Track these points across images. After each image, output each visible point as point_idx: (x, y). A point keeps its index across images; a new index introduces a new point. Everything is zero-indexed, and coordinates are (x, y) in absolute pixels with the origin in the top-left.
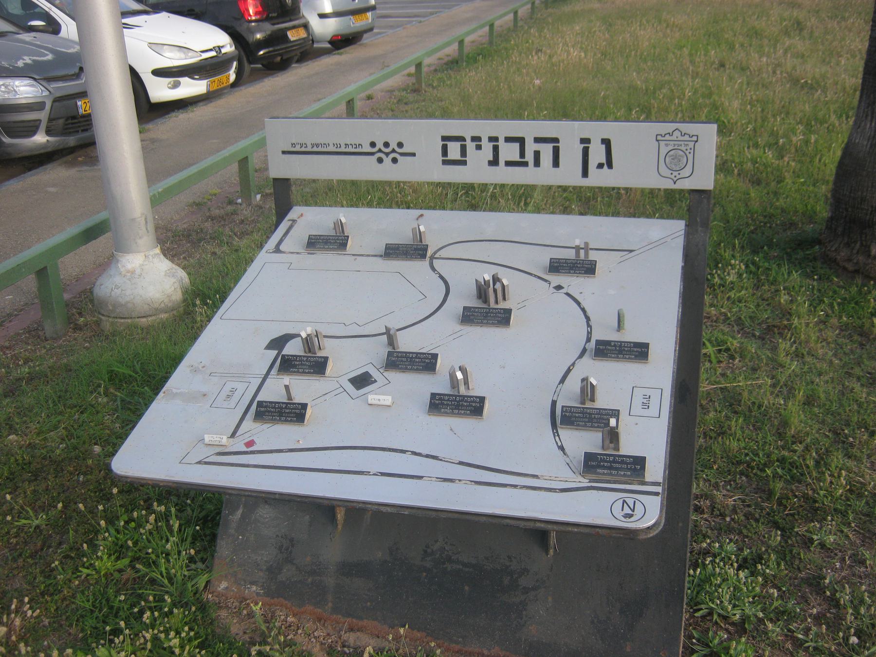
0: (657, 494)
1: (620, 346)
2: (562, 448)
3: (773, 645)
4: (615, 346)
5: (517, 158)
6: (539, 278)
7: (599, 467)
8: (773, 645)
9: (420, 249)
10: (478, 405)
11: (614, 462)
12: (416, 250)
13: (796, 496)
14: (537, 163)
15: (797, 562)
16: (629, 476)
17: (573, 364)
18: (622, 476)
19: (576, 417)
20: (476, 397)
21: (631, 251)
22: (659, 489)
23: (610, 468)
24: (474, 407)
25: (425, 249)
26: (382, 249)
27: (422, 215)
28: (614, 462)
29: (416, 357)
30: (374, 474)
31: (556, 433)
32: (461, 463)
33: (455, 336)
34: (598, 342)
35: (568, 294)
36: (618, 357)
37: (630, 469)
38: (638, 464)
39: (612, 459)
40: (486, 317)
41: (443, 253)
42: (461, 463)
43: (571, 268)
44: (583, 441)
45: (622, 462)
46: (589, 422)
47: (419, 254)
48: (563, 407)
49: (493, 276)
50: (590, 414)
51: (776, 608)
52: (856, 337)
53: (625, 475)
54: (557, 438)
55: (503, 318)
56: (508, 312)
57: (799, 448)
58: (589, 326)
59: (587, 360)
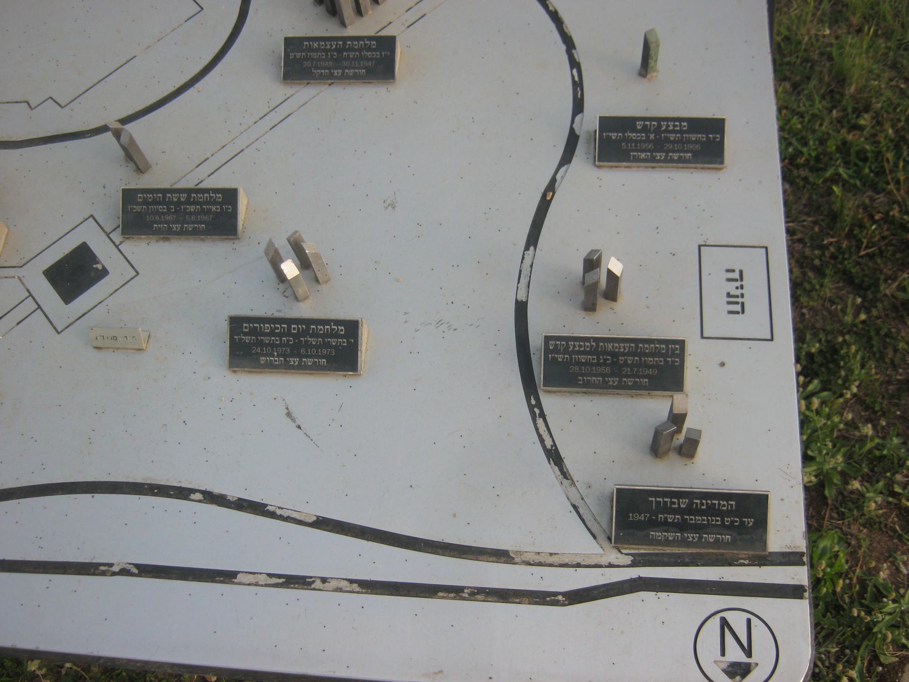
0: (795, 592)
2: (554, 456)
3: (870, 524)
4: (645, 129)
5: (117, 243)
7: (655, 524)
8: (870, 524)
10: (344, 342)
11: (690, 510)
13: (875, 222)
14: (729, 303)
15: (890, 353)
16: (727, 545)
17: (551, 187)
18: (708, 545)
19: (579, 363)
20: (338, 322)
22: (799, 575)
23: (682, 527)
24: (331, 347)
28: (690, 510)
29: (188, 202)
30: (124, 572)
31: (537, 411)
32: (322, 523)
33: (275, 117)
34: (607, 123)
36: (653, 160)
37: (731, 527)
38: (750, 510)
39: (684, 503)
42: (322, 523)
44: (603, 433)
45: (711, 511)
46: (613, 375)
48: (547, 339)
50: (614, 355)
51: (870, 451)
53: (717, 544)
54: (540, 422)
55: (375, 61)
56: (387, 44)
57: (865, 120)
58: (574, 64)
59: (581, 167)
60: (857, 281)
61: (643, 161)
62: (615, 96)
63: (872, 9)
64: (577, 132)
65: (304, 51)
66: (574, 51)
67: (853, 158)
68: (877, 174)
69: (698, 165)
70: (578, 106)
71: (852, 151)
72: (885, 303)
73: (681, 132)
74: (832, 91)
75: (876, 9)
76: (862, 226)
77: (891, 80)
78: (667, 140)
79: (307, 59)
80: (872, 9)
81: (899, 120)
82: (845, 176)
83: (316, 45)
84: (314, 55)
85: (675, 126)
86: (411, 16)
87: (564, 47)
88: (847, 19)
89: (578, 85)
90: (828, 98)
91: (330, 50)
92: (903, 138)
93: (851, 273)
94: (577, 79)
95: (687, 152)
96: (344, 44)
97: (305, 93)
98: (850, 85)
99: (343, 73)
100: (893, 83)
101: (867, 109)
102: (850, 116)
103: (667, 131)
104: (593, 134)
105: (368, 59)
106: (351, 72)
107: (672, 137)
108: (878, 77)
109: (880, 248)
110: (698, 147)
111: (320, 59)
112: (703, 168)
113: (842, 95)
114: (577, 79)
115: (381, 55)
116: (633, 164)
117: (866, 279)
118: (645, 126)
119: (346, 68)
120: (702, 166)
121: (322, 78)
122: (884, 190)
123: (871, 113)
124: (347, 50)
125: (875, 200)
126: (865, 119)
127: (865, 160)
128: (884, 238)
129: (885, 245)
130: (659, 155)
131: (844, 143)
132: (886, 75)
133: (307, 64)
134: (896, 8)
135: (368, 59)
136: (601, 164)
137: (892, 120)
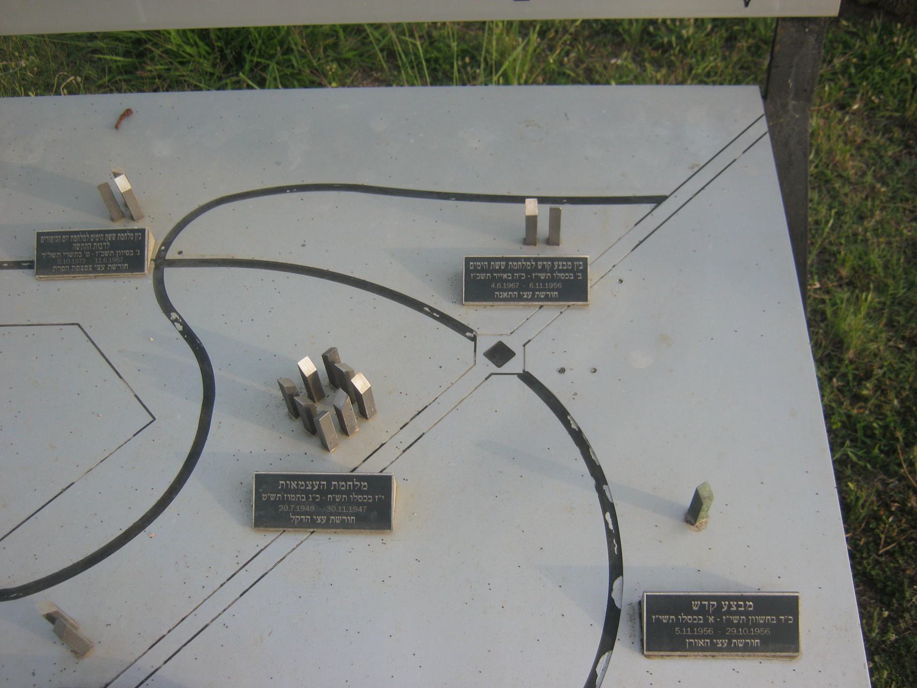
1: (718, 612)
4: (702, 611)
6: (445, 319)
9: (127, 244)
12: (109, 250)
21: (658, 200)
25: (137, 241)
26: (29, 253)
27: (128, 113)
33: (245, 579)
35: (527, 378)
40: (322, 504)
41: (188, 245)
43: (523, 285)
47: (126, 259)
49: (325, 357)
52: (897, 134)
55: (365, 504)
56: (381, 486)
58: (608, 506)
60: (879, 585)
61: (702, 649)
62: (664, 562)
63: (861, 259)
64: (617, 604)
65: (279, 492)
66: (605, 487)
67: (860, 434)
68: (887, 454)
69: (768, 654)
70: (616, 569)
71: (858, 426)
72: (913, 612)
73: (746, 613)
74: (829, 355)
75: (865, 259)
76: (878, 519)
77: (889, 340)
78: (730, 623)
79: (283, 501)
80: (861, 259)
81: (903, 388)
82: (854, 459)
83: (294, 484)
84: (292, 497)
85: (738, 606)
86: (407, 436)
87: (592, 482)
88: (836, 271)
89: (613, 536)
90: (826, 364)
91: (311, 492)
92: (909, 409)
93: (872, 576)
94: (611, 527)
95: (754, 637)
96: (329, 485)
97: (284, 542)
98: (848, 349)
99: (328, 520)
100: (891, 343)
101: (868, 376)
102: (851, 384)
103: (729, 612)
104: (637, 608)
105: (359, 504)
106: (337, 519)
107: (735, 619)
108: (875, 339)
109: (899, 544)
110: (767, 631)
111: (299, 503)
112: (774, 656)
113: (841, 360)
114: (611, 527)
115: (374, 498)
116: (689, 653)
117: (889, 583)
118: (702, 606)
119: (331, 514)
120: (773, 654)
121: (301, 525)
122: (896, 474)
123: (874, 380)
124: (332, 493)
125: (888, 484)
126: (867, 388)
127: (872, 436)
128: (903, 531)
129: (905, 539)
130: (721, 643)
131: (849, 416)
132: (884, 335)
133: (283, 508)
134: (884, 257)
135: (359, 504)
136: (651, 653)
137: (895, 388)
